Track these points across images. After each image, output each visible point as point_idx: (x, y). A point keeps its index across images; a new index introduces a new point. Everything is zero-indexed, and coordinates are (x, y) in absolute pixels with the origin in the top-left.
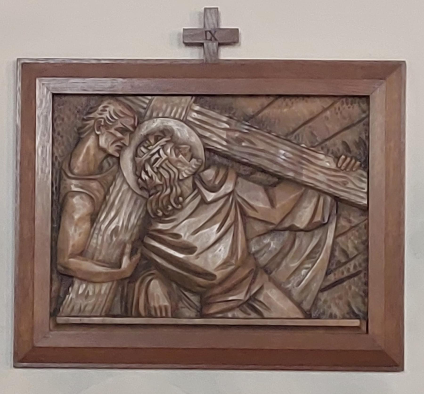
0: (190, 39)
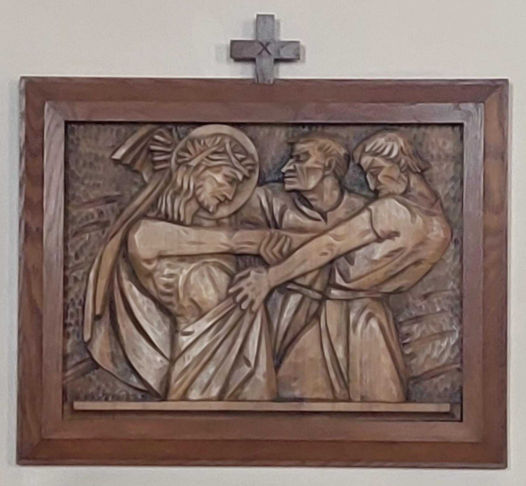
0: (238, 52)
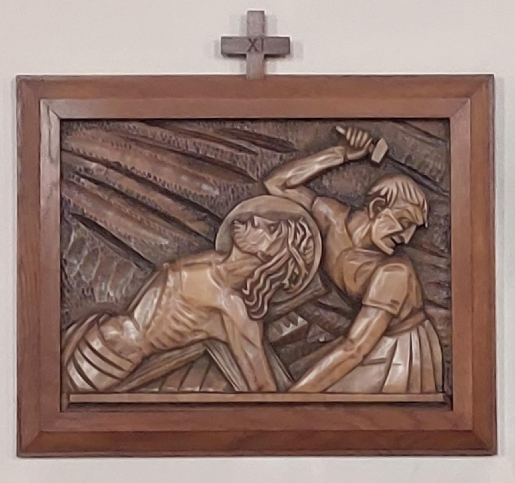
0: (229, 49)
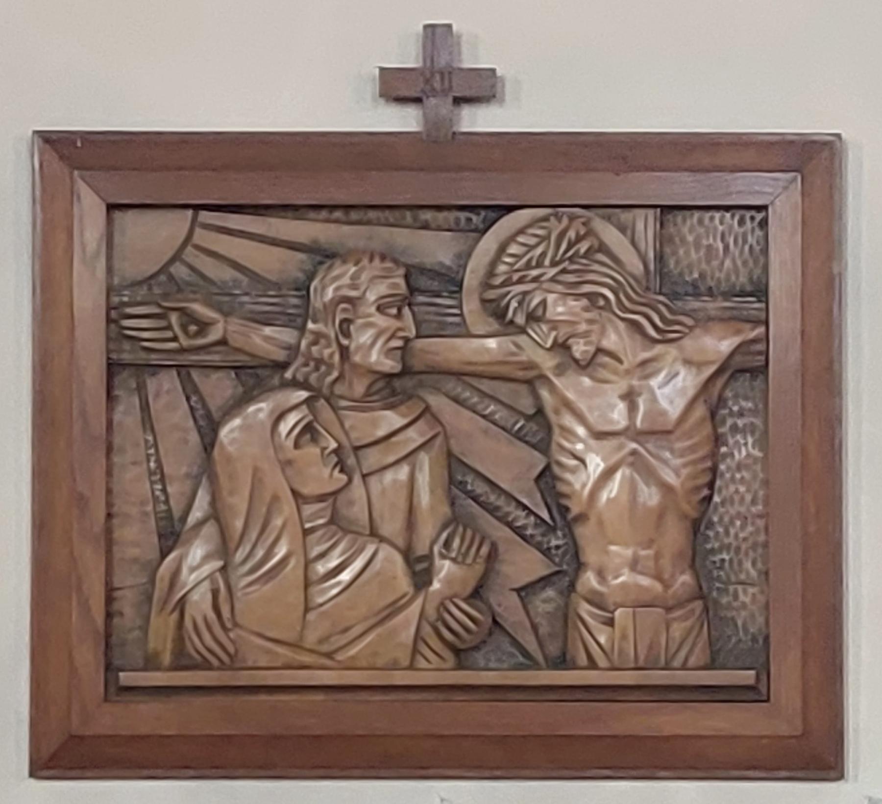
0: (395, 87)
